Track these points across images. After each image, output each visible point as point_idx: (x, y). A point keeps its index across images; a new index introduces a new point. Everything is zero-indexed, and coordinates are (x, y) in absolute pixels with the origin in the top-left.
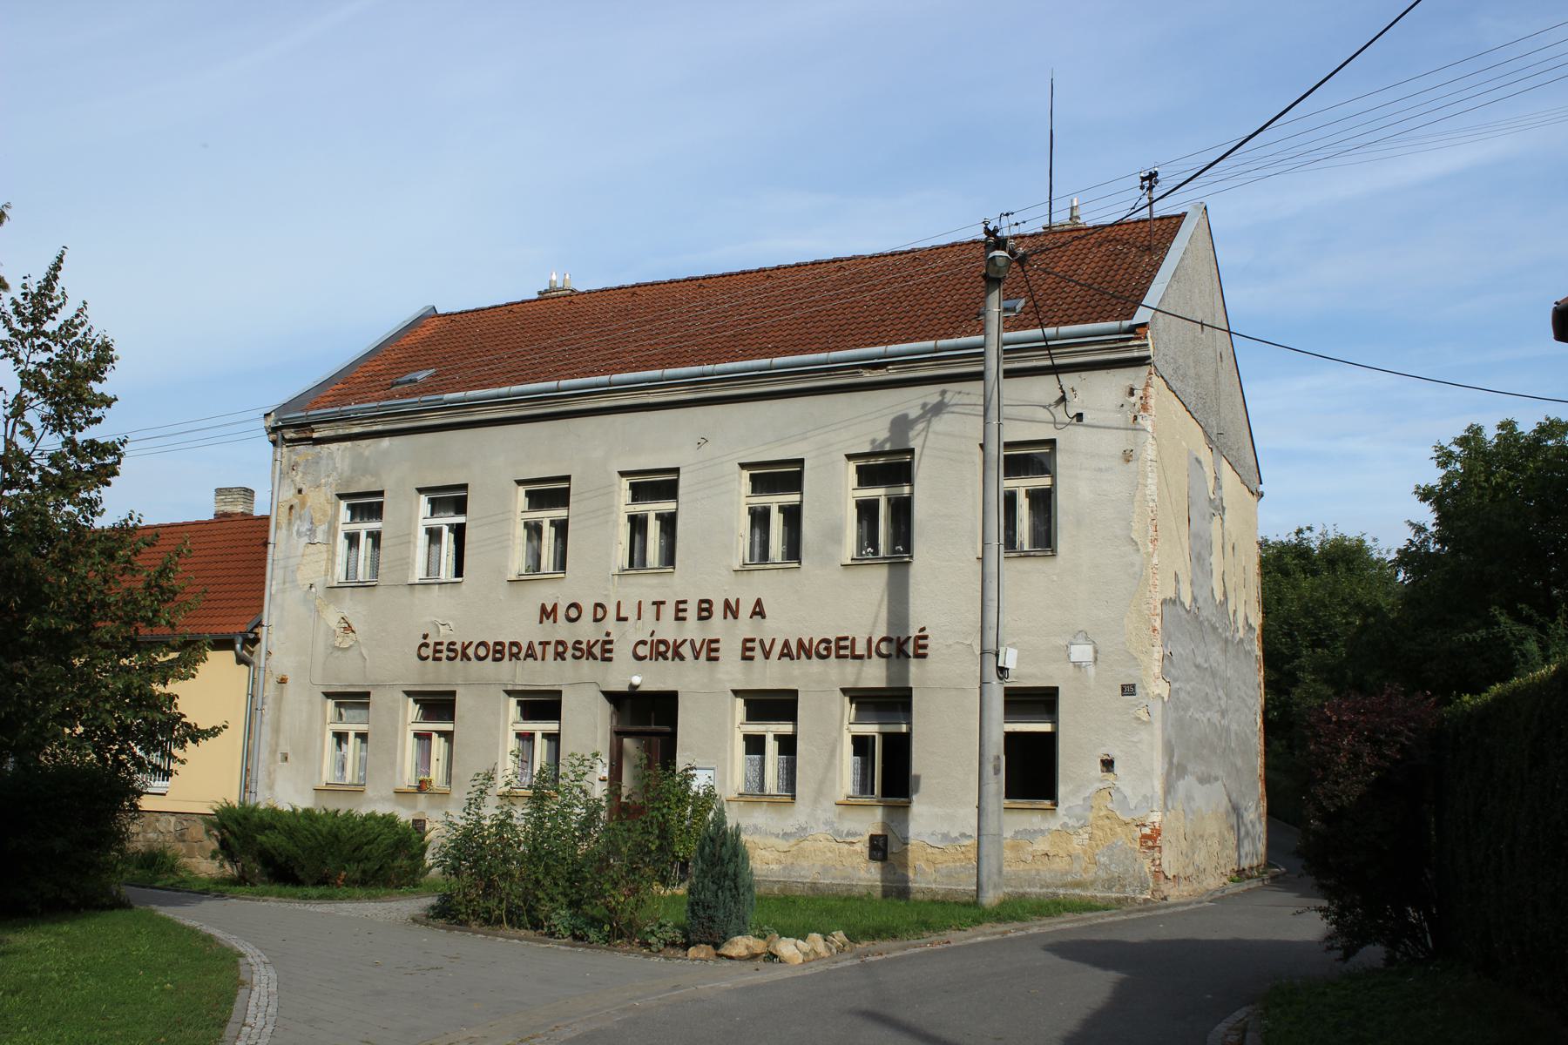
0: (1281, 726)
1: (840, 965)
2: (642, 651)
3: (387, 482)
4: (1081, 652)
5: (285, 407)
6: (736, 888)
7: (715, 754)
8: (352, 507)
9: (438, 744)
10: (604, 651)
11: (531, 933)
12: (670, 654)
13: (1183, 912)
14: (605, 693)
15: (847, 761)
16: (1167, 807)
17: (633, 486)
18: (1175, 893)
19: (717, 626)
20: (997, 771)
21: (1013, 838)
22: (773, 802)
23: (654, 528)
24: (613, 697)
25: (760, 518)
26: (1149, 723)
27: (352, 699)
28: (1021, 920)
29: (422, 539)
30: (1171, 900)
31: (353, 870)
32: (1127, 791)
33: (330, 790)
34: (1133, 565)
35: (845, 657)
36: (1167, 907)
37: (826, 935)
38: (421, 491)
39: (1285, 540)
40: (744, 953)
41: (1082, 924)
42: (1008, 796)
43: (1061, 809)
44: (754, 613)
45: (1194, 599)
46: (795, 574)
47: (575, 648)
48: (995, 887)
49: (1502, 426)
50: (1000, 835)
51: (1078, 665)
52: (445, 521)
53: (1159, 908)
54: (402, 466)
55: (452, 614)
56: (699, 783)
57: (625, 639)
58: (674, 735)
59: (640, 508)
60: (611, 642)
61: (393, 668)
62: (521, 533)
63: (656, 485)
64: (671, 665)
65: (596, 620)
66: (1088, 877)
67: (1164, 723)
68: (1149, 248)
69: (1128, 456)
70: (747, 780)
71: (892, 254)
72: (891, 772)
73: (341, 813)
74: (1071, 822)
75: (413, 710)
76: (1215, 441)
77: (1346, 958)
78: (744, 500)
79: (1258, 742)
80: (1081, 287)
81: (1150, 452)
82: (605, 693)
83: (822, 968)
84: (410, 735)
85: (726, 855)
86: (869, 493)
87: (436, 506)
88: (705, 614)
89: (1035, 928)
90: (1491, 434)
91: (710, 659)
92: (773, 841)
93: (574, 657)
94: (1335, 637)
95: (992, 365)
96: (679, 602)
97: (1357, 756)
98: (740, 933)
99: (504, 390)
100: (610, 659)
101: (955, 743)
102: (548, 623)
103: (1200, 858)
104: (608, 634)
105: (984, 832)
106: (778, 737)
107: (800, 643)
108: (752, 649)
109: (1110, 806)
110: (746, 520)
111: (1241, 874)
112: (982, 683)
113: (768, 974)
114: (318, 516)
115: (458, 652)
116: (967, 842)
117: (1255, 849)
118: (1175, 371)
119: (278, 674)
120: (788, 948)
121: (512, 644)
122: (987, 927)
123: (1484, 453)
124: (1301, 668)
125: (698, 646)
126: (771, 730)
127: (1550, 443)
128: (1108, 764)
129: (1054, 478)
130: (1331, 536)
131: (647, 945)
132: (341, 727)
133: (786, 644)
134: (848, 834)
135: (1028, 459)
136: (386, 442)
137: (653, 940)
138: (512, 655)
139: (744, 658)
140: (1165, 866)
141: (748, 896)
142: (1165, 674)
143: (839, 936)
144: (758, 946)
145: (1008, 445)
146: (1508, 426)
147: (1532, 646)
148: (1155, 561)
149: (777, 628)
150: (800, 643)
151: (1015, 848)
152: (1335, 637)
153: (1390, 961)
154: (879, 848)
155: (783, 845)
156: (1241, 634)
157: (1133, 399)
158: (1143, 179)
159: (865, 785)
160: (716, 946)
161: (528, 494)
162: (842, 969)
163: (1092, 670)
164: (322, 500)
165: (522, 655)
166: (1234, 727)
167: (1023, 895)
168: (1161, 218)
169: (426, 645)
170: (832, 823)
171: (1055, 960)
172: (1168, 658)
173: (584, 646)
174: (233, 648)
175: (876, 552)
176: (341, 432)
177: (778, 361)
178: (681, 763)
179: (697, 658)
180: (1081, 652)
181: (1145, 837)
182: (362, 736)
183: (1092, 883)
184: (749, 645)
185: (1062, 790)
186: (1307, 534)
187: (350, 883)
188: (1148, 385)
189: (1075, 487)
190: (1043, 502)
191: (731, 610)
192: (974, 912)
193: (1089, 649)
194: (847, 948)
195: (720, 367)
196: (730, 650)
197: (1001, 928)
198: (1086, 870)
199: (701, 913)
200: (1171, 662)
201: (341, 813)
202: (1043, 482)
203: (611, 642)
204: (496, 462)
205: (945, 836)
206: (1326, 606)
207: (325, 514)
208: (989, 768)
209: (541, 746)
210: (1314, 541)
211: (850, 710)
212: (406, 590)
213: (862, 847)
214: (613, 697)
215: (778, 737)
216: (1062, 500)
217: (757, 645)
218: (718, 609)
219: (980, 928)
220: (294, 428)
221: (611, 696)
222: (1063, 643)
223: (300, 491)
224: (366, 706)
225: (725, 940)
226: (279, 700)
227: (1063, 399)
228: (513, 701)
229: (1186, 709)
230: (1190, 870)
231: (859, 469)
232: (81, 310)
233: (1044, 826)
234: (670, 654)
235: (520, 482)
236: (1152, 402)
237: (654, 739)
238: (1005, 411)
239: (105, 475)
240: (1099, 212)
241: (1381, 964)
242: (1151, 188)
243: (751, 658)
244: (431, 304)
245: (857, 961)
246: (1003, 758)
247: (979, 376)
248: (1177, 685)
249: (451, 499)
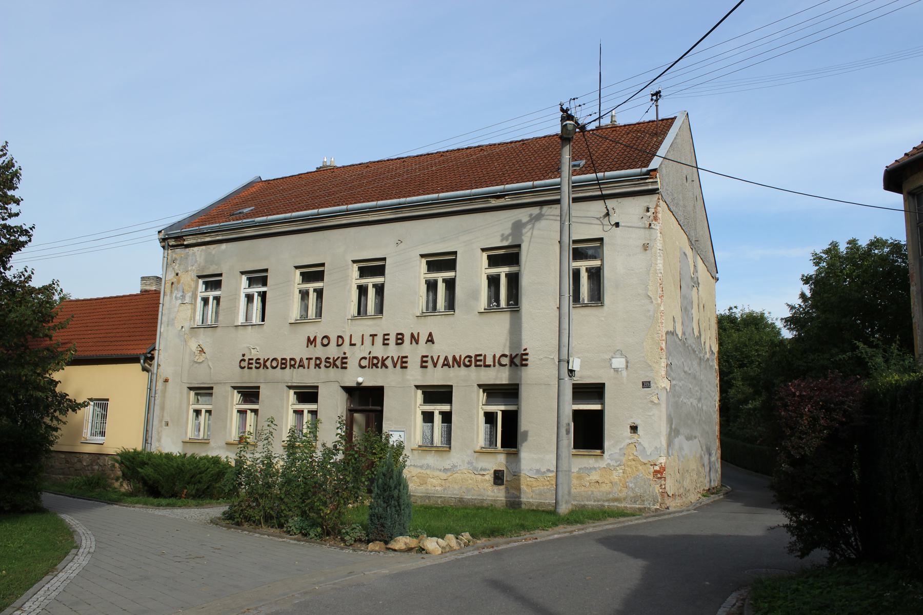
0: (726, 409)
1: (465, 555)
2: (364, 363)
3: (224, 269)
4: (619, 363)
5: (172, 227)
6: (399, 505)
7: (404, 423)
8: (206, 283)
9: (250, 416)
10: (342, 363)
11: (278, 531)
12: (379, 365)
13: (679, 517)
14: (343, 387)
15: (482, 426)
16: (665, 452)
17: (360, 269)
18: (673, 505)
19: (407, 348)
20: (568, 432)
21: (578, 472)
22: (438, 450)
23: (371, 292)
24: (348, 390)
25: (432, 286)
26: (659, 404)
27: (203, 391)
28: (582, 523)
29: (243, 300)
30: (671, 509)
31: (191, 489)
32: (646, 445)
33: (191, 442)
34: (649, 311)
35: (480, 366)
36: (670, 513)
37: (457, 534)
38: (242, 273)
39: (723, 313)
40: (404, 547)
41: (619, 525)
42: (575, 448)
43: (606, 455)
44: (428, 341)
45: (684, 333)
46: (450, 318)
47: (326, 362)
48: (566, 502)
49: (849, 243)
50: (570, 471)
51: (616, 370)
52: (256, 290)
53: (664, 514)
54: (231, 259)
55: (256, 343)
56: (394, 439)
57: (354, 355)
58: (382, 411)
59: (364, 281)
60: (346, 358)
61: (226, 372)
62: (297, 296)
63: (373, 268)
64: (380, 371)
65: (338, 345)
66: (622, 495)
67: (667, 405)
68: (656, 134)
69: (646, 247)
70: (423, 438)
71: (511, 143)
72: (509, 433)
73: (188, 455)
74: (612, 463)
75: (237, 397)
76: (694, 244)
77: (802, 557)
78: (422, 276)
79: (716, 417)
80: (618, 155)
81: (659, 245)
82: (343, 387)
83: (453, 557)
84: (235, 412)
85: (392, 483)
86: (494, 271)
87: (252, 282)
88: (400, 341)
89: (591, 528)
90: (843, 248)
91: (402, 367)
92: (437, 473)
93: (326, 367)
94: (752, 362)
95: (566, 194)
96: (385, 335)
97: (815, 419)
98: (401, 534)
99: (288, 215)
100: (346, 368)
101: (545, 414)
102: (311, 347)
103: (687, 483)
104: (345, 353)
105: (560, 469)
106: (441, 413)
107: (454, 358)
108: (426, 362)
109: (635, 453)
110: (424, 287)
111: (710, 491)
112: (559, 379)
113: (413, 563)
114: (186, 288)
115: (261, 364)
116: (551, 475)
117: (716, 478)
118: (673, 199)
119: (163, 377)
120: (431, 544)
121: (291, 359)
122: (561, 528)
123: (840, 257)
124: (734, 379)
125: (395, 360)
126: (437, 409)
127: (876, 251)
128: (634, 429)
129: (602, 260)
130: (747, 311)
131: (343, 540)
132: (198, 407)
133: (446, 358)
134: (481, 470)
135: (585, 250)
136: (224, 246)
137: (347, 538)
138: (291, 366)
139: (422, 367)
140: (668, 489)
141: (407, 511)
142: (668, 376)
143: (466, 536)
144: (413, 542)
145: (575, 242)
146: (853, 242)
147: (879, 360)
148: (662, 308)
149: (441, 349)
150: (454, 358)
151: (579, 478)
152: (752, 362)
153: (832, 560)
154: (498, 477)
155: (443, 475)
156: (708, 355)
157: (649, 214)
158: (653, 95)
159: (492, 441)
160: (386, 543)
161: (302, 274)
162: (466, 558)
163: (624, 373)
164: (189, 279)
165: (297, 366)
166: (704, 408)
167: (584, 506)
168: (662, 120)
169: (244, 360)
170: (472, 463)
171: (603, 550)
172: (669, 365)
173: (331, 360)
174: (139, 362)
175: (498, 305)
176: (199, 241)
177: (442, 195)
178: (385, 428)
179: (395, 367)
180: (619, 363)
181: (656, 472)
182: (209, 412)
183: (624, 499)
184: (425, 359)
185: (607, 444)
186: (734, 310)
187: (188, 496)
188: (657, 206)
189: (616, 264)
190: (596, 275)
191: (415, 339)
192: (553, 518)
193: (623, 360)
194: (471, 543)
195: (409, 199)
196: (414, 363)
197: (569, 528)
198: (621, 491)
199: (376, 521)
200: (671, 368)
201: (188, 455)
202: (596, 263)
203: (346, 358)
204: (284, 256)
205: (538, 471)
206: (746, 346)
207: (190, 287)
208: (563, 431)
209: (307, 417)
210: (738, 313)
211: (482, 396)
212: (233, 329)
213: (489, 477)
214: (348, 390)
215: (441, 413)
216: (607, 274)
217: (429, 359)
218: (407, 339)
219: (556, 529)
220: (174, 240)
221: (347, 389)
222: (608, 357)
223: (177, 274)
224: (211, 394)
225: (391, 538)
226: (164, 391)
227: (608, 214)
228: (292, 392)
229: (679, 397)
230: (681, 491)
231: (489, 257)
232: (4, 147)
233: (596, 465)
234: (379, 365)
235: (297, 267)
236: (660, 215)
237: (371, 414)
238: (573, 219)
239: (17, 246)
240: (627, 117)
241: (825, 562)
242: (657, 100)
243: (426, 367)
244: (258, 175)
245: (476, 552)
246: (572, 425)
247: (558, 202)
248: (674, 382)
249: (258, 278)
